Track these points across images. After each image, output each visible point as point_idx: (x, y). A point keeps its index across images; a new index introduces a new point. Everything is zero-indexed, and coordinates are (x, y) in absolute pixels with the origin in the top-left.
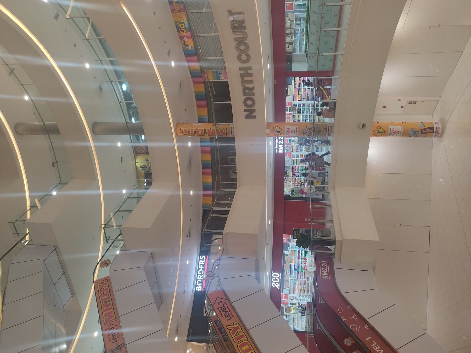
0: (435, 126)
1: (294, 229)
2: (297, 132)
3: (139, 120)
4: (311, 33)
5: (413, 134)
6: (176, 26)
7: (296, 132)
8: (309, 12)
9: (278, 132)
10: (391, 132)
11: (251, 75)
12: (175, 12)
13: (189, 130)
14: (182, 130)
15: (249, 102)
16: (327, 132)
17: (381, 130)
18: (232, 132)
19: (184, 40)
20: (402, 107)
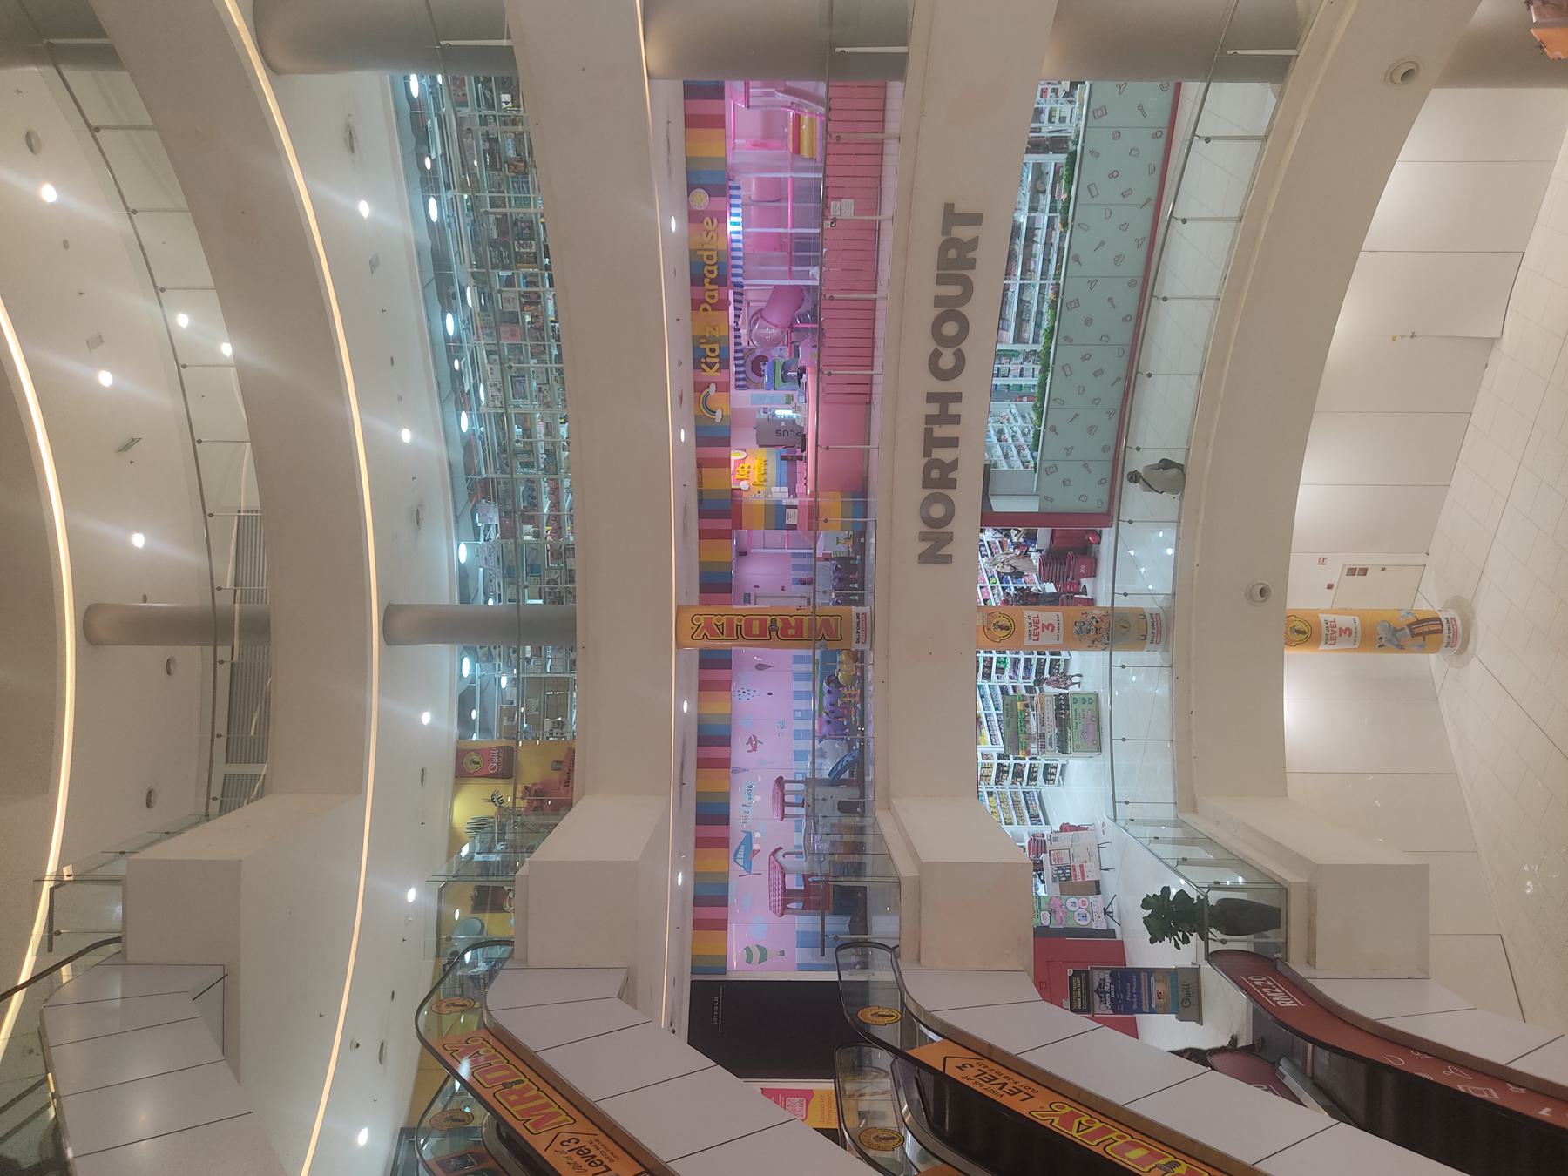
0: (1442, 616)
1: (1070, 972)
2: (1062, 628)
3: (492, 658)
4: (1055, 400)
5: (1389, 637)
6: (695, 349)
7: (1056, 628)
8: (1051, 343)
9: (1002, 629)
10: (1330, 632)
11: (955, 420)
12: (701, 309)
13: (719, 620)
14: (698, 620)
15: (937, 511)
16: (1150, 630)
17: (1300, 626)
18: (858, 628)
19: (707, 391)
20: (1330, 587)
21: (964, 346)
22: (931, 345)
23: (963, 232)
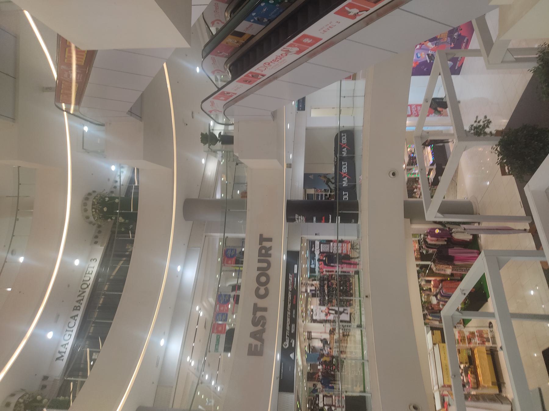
21: (268, 286)
22: (256, 285)
23: (267, 244)
